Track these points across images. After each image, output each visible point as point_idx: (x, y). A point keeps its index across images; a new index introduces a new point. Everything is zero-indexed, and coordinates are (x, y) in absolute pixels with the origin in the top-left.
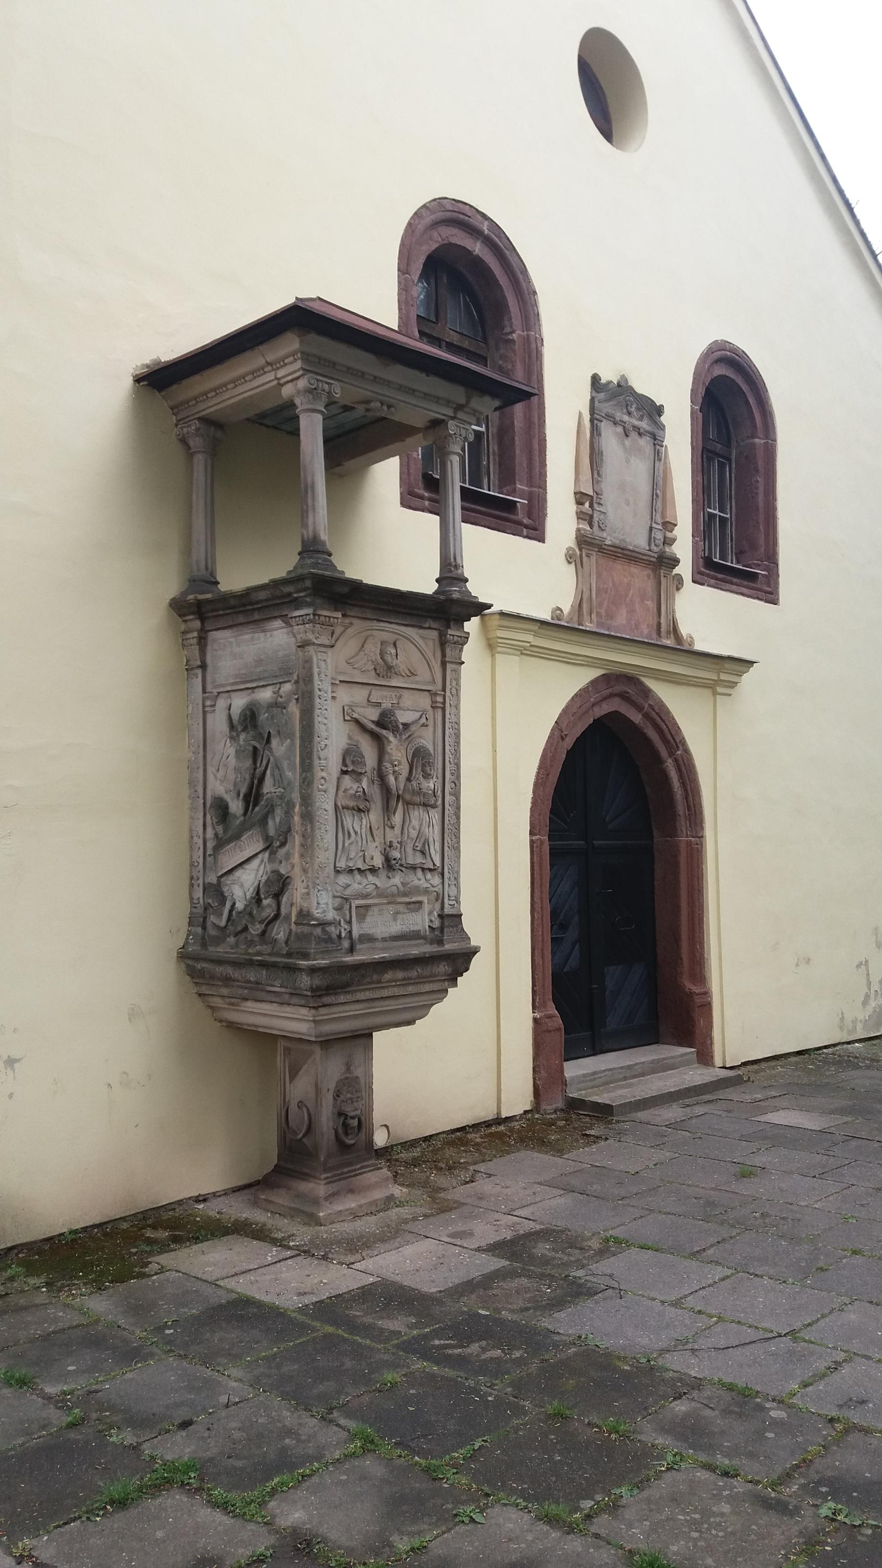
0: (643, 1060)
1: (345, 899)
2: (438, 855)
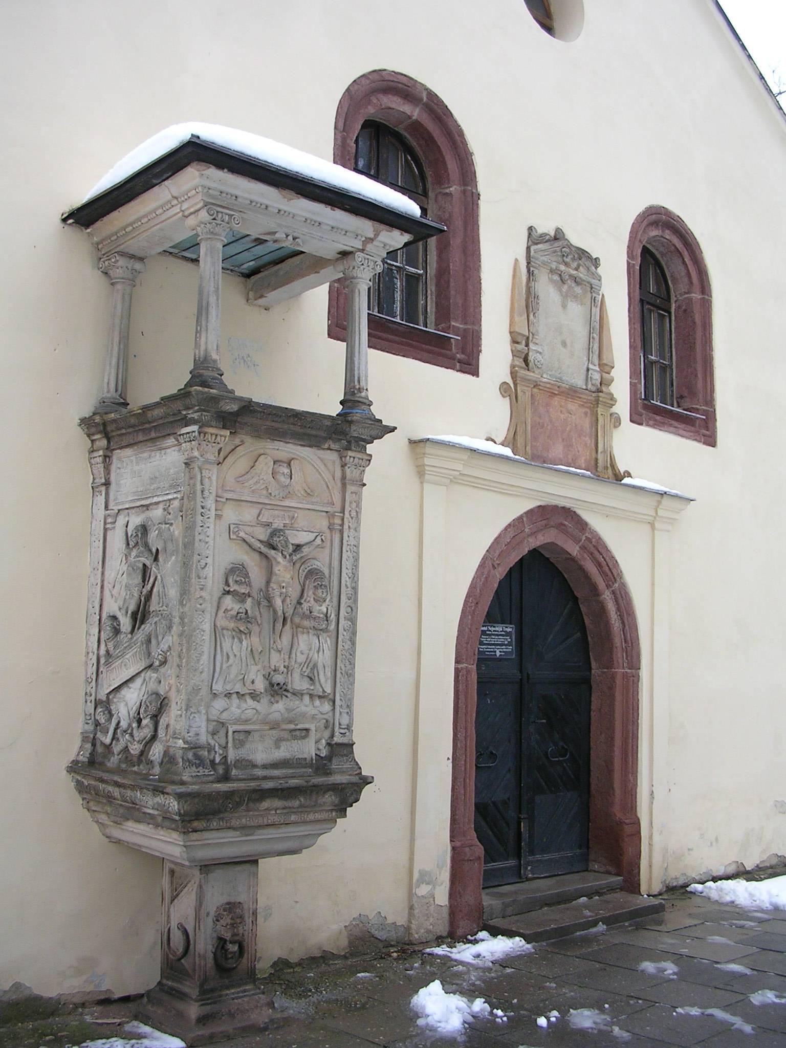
1: (222, 723)
2: (329, 681)
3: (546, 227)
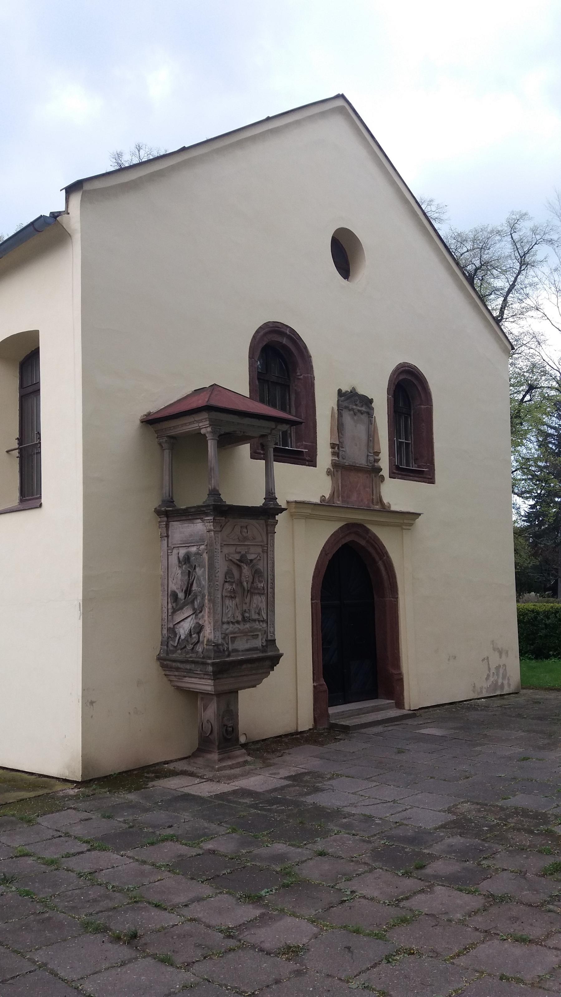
0: (368, 706)
3: (346, 388)
